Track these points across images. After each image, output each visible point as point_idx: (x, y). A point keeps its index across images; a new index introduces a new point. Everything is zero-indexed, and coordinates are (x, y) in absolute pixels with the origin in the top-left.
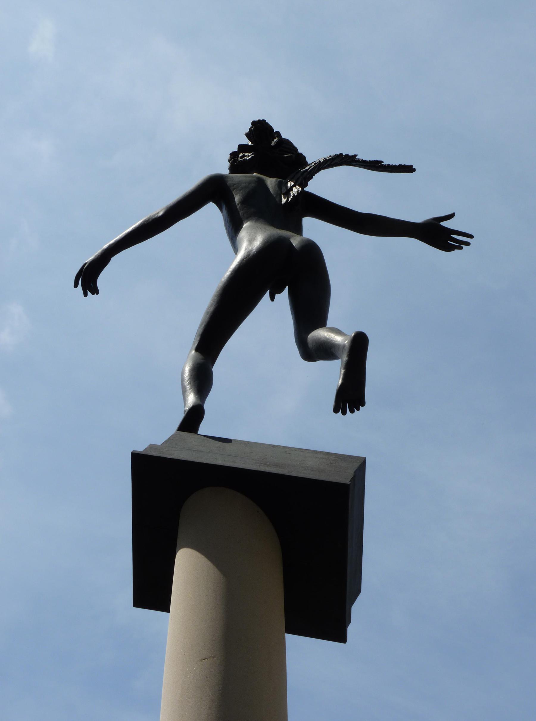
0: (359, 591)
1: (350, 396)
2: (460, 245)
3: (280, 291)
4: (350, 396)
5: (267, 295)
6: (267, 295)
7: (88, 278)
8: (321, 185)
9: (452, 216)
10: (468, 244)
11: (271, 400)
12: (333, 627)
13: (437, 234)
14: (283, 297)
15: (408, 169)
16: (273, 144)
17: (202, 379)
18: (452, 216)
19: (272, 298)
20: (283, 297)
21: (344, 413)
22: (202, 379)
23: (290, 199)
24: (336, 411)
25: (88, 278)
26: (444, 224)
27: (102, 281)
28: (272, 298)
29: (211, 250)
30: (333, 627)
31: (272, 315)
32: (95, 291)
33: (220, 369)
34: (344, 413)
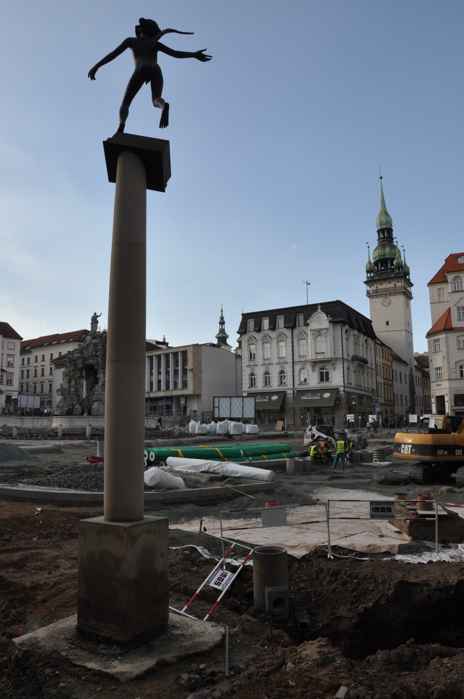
0: (170, 176)
1: (164, 122)
2: (208, 60)
3: (148, 82)
4: (164, 122)
5: (145, 83)
6: (145, 83)
7: (92, 74)
8: (164, 40)
9: (205, 50)
10: (211, 59)
11: (143, 122)
12: (161, 187)
13: (200, 56)
14: (149, 84)
15: (193, 33)
16: (302, 398)
17: (124, 113)
18: (205, 50)
19: (147, 84)
20: (149, 84)
21: (162, 128)
22: (124, 113)
23: (399, 557)
24: (160, 127)
25: (92, 74)
26: (203, 53)
27: (96, 76)
28: (147, 84)
29: (127, 63)
30: (161, 187)
31: (146, 89)
32: (95, 79)
33: (131, 109)
34: (162, 128)
